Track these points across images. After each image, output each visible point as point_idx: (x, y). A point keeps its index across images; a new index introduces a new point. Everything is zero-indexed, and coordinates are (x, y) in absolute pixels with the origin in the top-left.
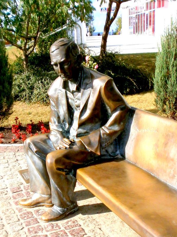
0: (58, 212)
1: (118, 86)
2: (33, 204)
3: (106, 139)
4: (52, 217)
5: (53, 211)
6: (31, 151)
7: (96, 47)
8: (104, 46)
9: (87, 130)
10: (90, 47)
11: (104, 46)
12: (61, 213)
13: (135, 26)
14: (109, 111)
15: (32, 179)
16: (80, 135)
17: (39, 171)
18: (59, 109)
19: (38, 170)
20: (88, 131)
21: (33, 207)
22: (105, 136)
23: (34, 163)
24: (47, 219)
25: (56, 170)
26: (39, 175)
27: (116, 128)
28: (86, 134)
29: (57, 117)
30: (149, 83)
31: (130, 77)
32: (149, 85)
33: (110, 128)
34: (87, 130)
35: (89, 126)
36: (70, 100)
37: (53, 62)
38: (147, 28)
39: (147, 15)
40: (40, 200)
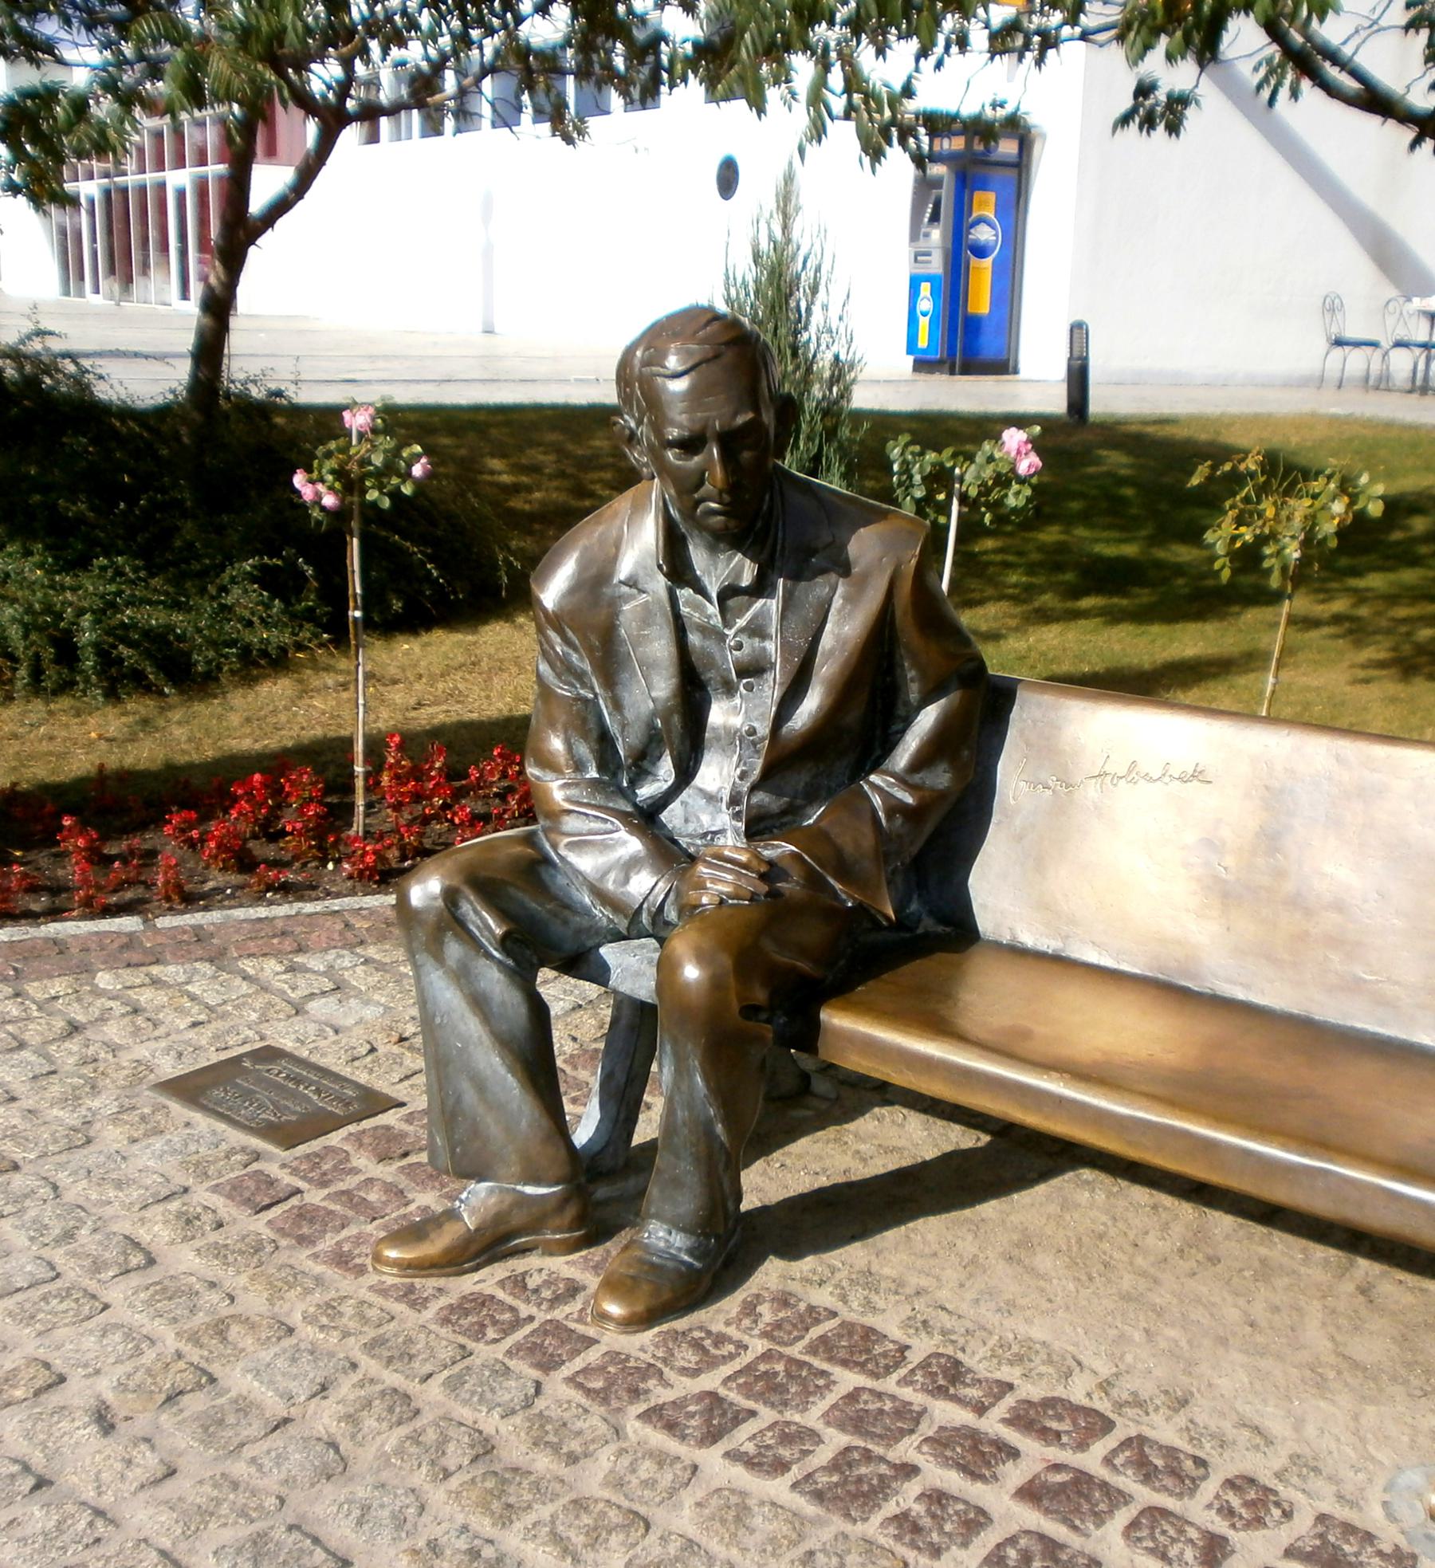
0: (683, 1262)
1: (337, 580)
2: (474, 1248)
3: (900, 836)
4: (666, 1295)
5: (653, 1265)
6: (466, 937)
7: (146, 357)
8: (210, 349)
9: (795, 797)
10: (87, 355)
11: (210, 349)
12: (697, 1264)
13: (99, 246)
14: (914, 692)
15: (459, 1100)
16: (762, 826)
17: (511, 1051)
18: (619, 689)
19: (503, 1042)
20: (799, 802)
21: (476, 1269)
22: (899, 820)
23: (479, 1003)
24: (640, 1308)
25: (740, 1019)
26: (511, 1070)
27: (941, 778)
28: (785, 820)
29: (595, 734)
30: (496, 568)
31: (404, 537)
32: (500, 578)
33: (917, 778)
34: (795, 797)
35: (800, 779)
36: (694, 639)
37: (673, 424)
38: (145, 266)
39: (181, 195)
40: (517, 1219)
